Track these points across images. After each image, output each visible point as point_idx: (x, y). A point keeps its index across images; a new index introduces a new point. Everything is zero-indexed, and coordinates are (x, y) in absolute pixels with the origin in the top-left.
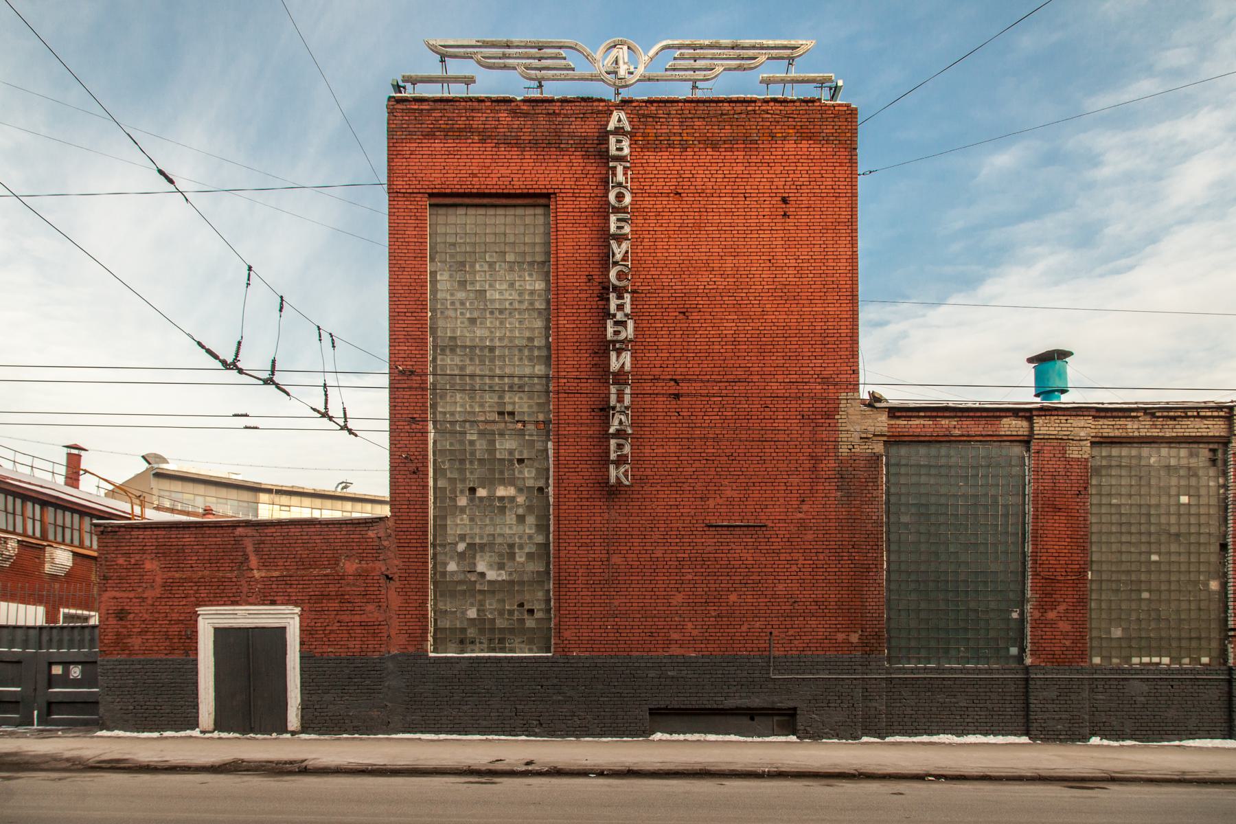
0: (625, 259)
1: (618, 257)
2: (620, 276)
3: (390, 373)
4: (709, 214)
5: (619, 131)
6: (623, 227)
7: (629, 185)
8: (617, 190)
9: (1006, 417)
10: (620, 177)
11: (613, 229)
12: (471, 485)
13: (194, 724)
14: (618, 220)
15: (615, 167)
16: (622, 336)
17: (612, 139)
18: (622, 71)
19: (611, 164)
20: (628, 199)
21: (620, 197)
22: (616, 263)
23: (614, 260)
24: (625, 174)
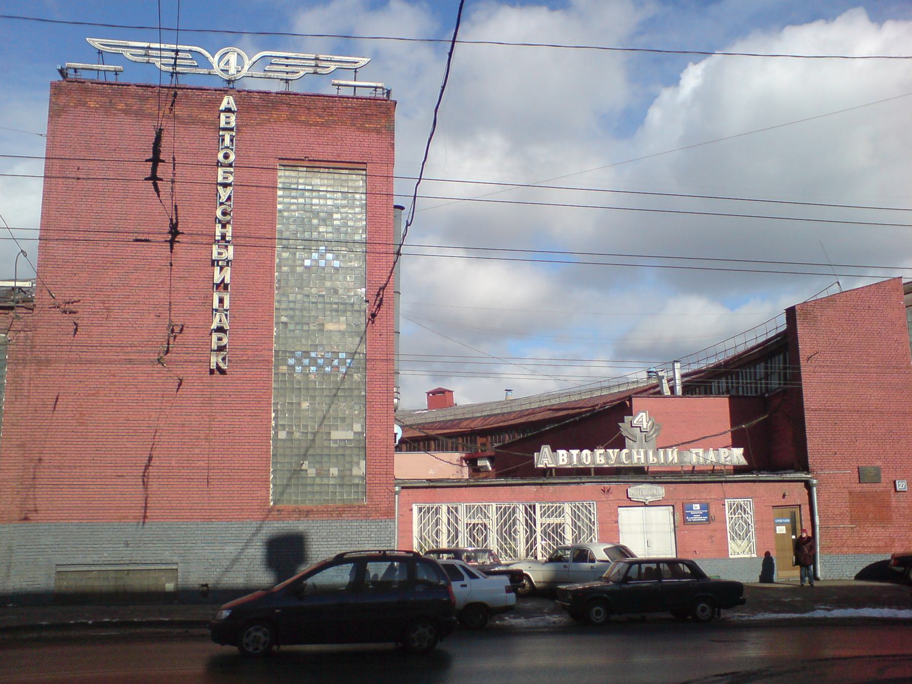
0: (229, 199)
1: (224, 199)
2: (224, 213)
3: (45, 177)
4: (207, 453)
5: (228, 110)
6: (254, 650)
7: (234, 147)
8: (225, 151)
9: (541, 627)
10: (227, 142)
11: (220, 180)
12: (208, 373)
13: (590, 474)
14: (224, 172)
15: (224, 136)
16: (224, 256)
17: (223, 116)
18: (232, 71)
19: (221, 133)
20: (232, 157)
21: (226, 156)
22: (221, 204)
23: (221, 201)
24: (232, 140)
